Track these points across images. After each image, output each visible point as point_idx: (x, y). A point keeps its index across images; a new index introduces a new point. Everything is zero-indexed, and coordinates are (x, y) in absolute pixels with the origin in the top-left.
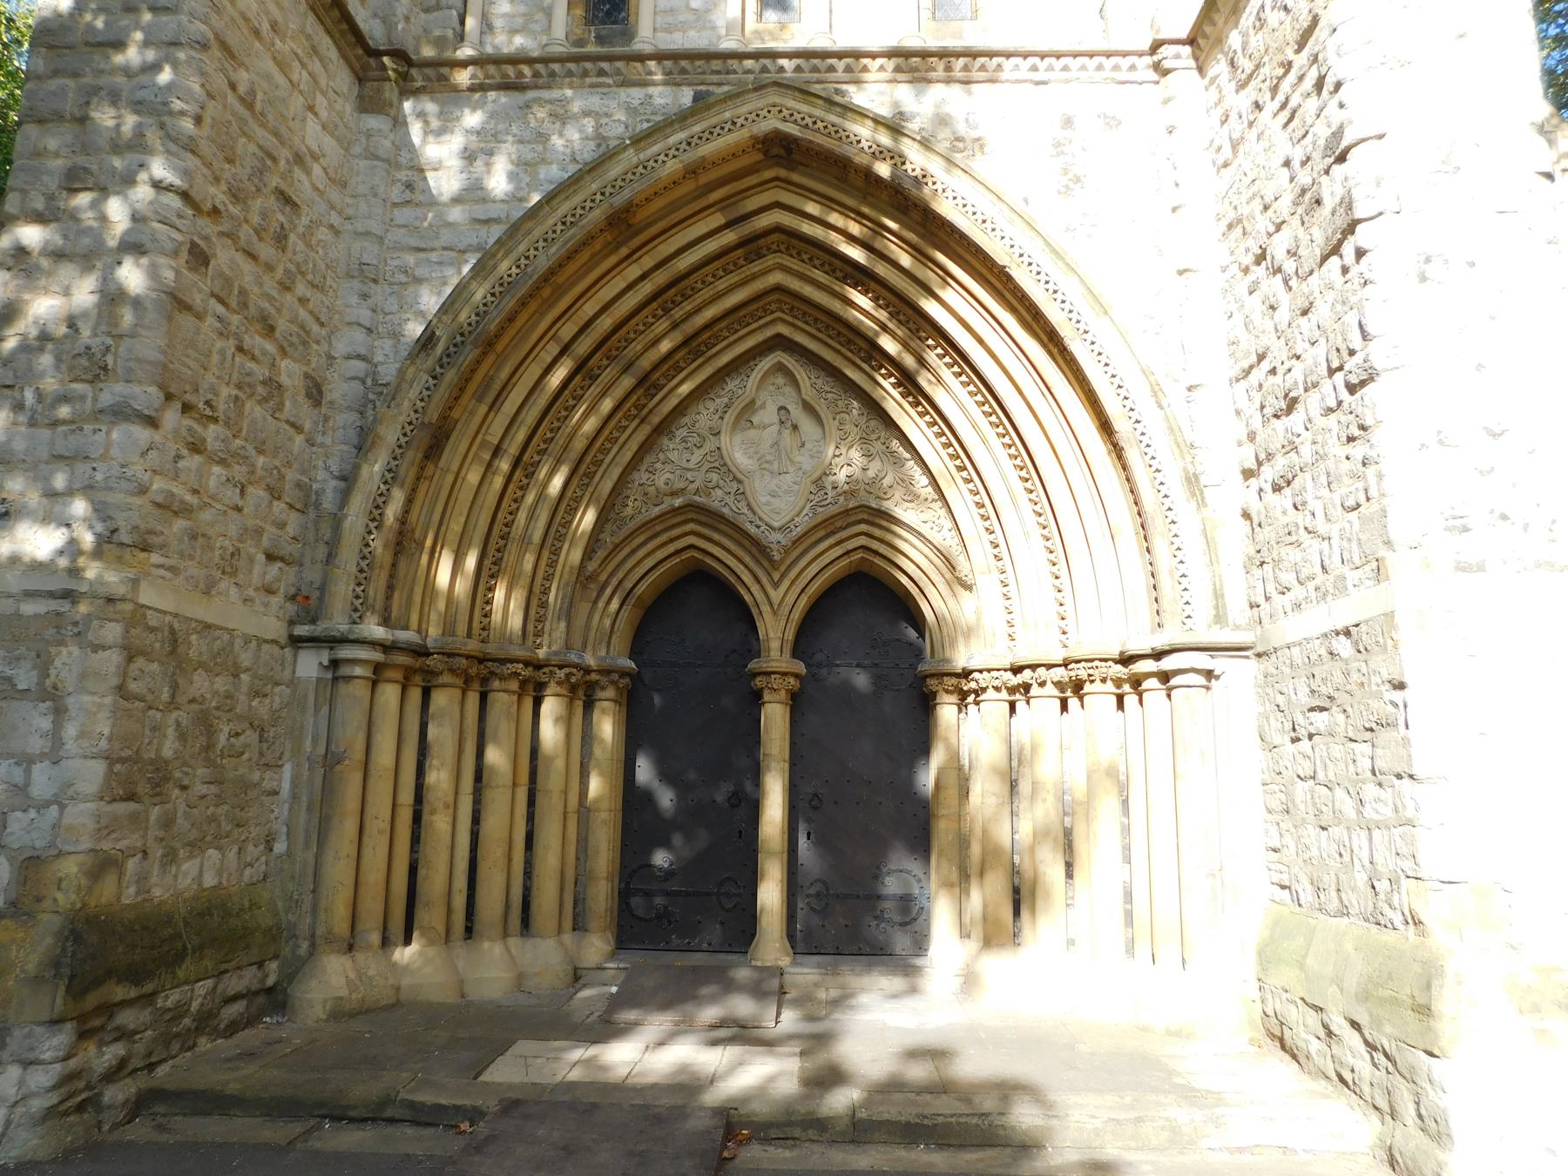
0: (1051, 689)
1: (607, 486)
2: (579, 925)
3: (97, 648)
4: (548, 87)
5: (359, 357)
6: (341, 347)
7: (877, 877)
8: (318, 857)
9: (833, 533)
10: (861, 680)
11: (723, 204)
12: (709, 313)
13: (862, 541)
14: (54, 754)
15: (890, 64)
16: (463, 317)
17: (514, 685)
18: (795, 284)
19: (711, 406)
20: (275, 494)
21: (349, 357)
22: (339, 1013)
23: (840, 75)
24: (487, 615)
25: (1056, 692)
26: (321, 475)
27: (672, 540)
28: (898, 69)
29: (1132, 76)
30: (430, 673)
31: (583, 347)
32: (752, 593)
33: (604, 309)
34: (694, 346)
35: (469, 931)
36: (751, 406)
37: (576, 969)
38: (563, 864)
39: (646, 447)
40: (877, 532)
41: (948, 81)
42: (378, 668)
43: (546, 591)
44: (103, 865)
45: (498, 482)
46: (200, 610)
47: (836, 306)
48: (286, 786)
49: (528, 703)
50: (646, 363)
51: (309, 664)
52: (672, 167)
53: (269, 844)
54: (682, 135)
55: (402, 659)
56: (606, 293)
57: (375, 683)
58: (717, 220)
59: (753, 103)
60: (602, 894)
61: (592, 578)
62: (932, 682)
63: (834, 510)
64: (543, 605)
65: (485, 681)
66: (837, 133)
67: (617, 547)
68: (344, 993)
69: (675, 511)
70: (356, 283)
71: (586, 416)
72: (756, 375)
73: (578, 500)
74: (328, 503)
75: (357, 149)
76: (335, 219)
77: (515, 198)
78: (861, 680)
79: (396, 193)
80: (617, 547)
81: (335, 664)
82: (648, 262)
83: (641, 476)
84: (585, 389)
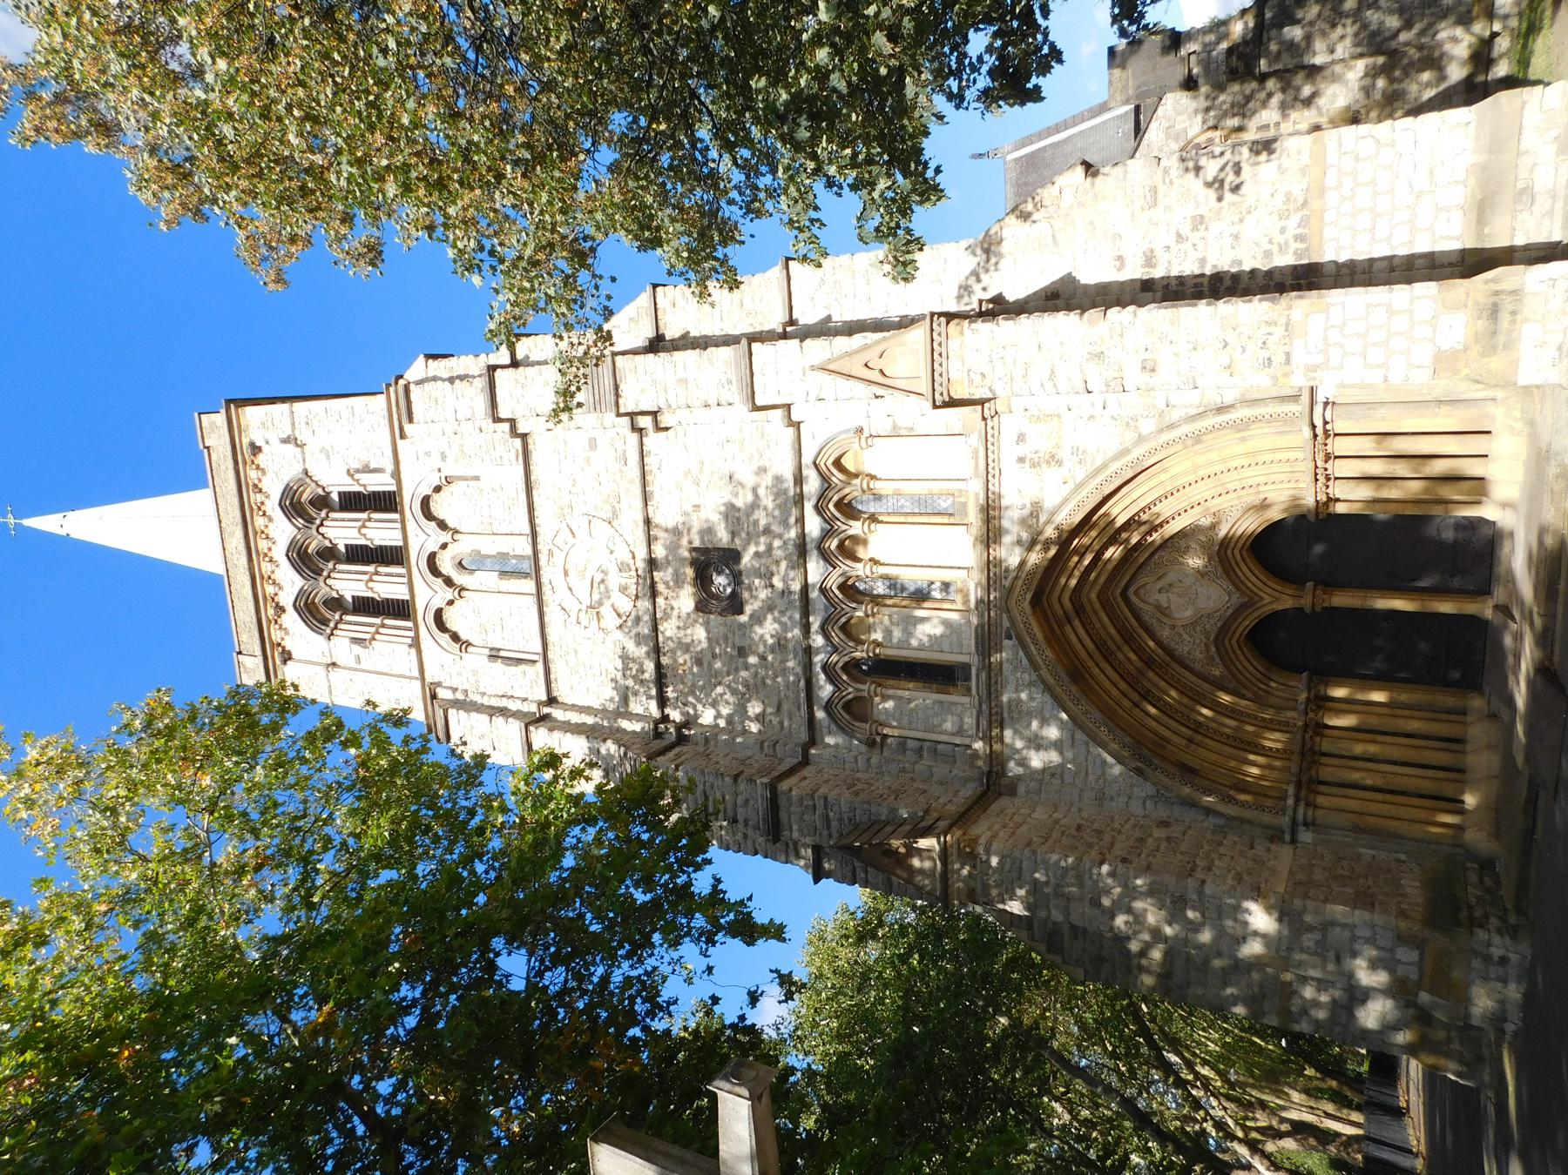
0: (1329, 465)
1: (1206, 686)
2: (1463, 712)
3: (1305, 907)
4: (1002, 708)
5: (1144, 803)
6: (1139, 811)
7: (1442, 543)
8: (1409, 839)
9: (1232, 568)
10: (1319, 549)
11: (1061, 626)
12: (1113, 631)
13: (1237, 552)
14: (1352, 927)
15: (993, 546)
16: (1126, 754)
17: (1318, 739)
18: (1098, 588)
19: (1157, 629)
20: (1220, 844)
21: (1145, 808)
22: (1497, 835)
23: (998, 570)
24: (1278, 750)
25: (1331, 462)
26: (1206, 824)
27: (1234, 651)
28: (995, 543)
29: (996, 428)
30: (1310, 781)
31: (1136, 697)
32: (1267, 610)
33: (1115, 685)
34: (1129, 639)
35: (1460, 771)
36: (1159, 608)
37: (1488, 716)
38: (1421, 719)
39: (1187, 668)
40: (1232, 544)
41: (1000, 518)
42: (1308, 805)
43: (1264, 719)
44: (1403, 914)
45: (1210, 742)
46: (1285, 874)
47: (1110, 567)
48: (1372, 852)
49: (1327, 732)
50: (1140, 665)
51: (1306, 836)
52: (1049, 652)
53: (1399, 861)
54: (1033, 648)
55: (1303, 793)
56: (1107, 684)
57: (1316, 807)
58: (1068, 628)
59: (1015, 612)
60: (1448, 700)
61: (1255, 694)
62: (1321, 516)
63: (1219, 568)
64: (1271, 721)
65: (1314, 753)
66: (1032, 573)
67: (1238, 681)
68: (1485, 833)
69: (1218, 651)
70: (1106, 802)
71: (1169, 696)
72: (1141, 605)
73: (1213, 700)
74: (1221, 822)
75: (1036, 798)
76: (1074, 810)
77: (1062, 723)
78: (1319, 549)
79: (1056, 782)
80: (1238, 681)
81: (1305, 824)
82: (1090, 663)
83: (1197, 666)
84: (1154, 695)
